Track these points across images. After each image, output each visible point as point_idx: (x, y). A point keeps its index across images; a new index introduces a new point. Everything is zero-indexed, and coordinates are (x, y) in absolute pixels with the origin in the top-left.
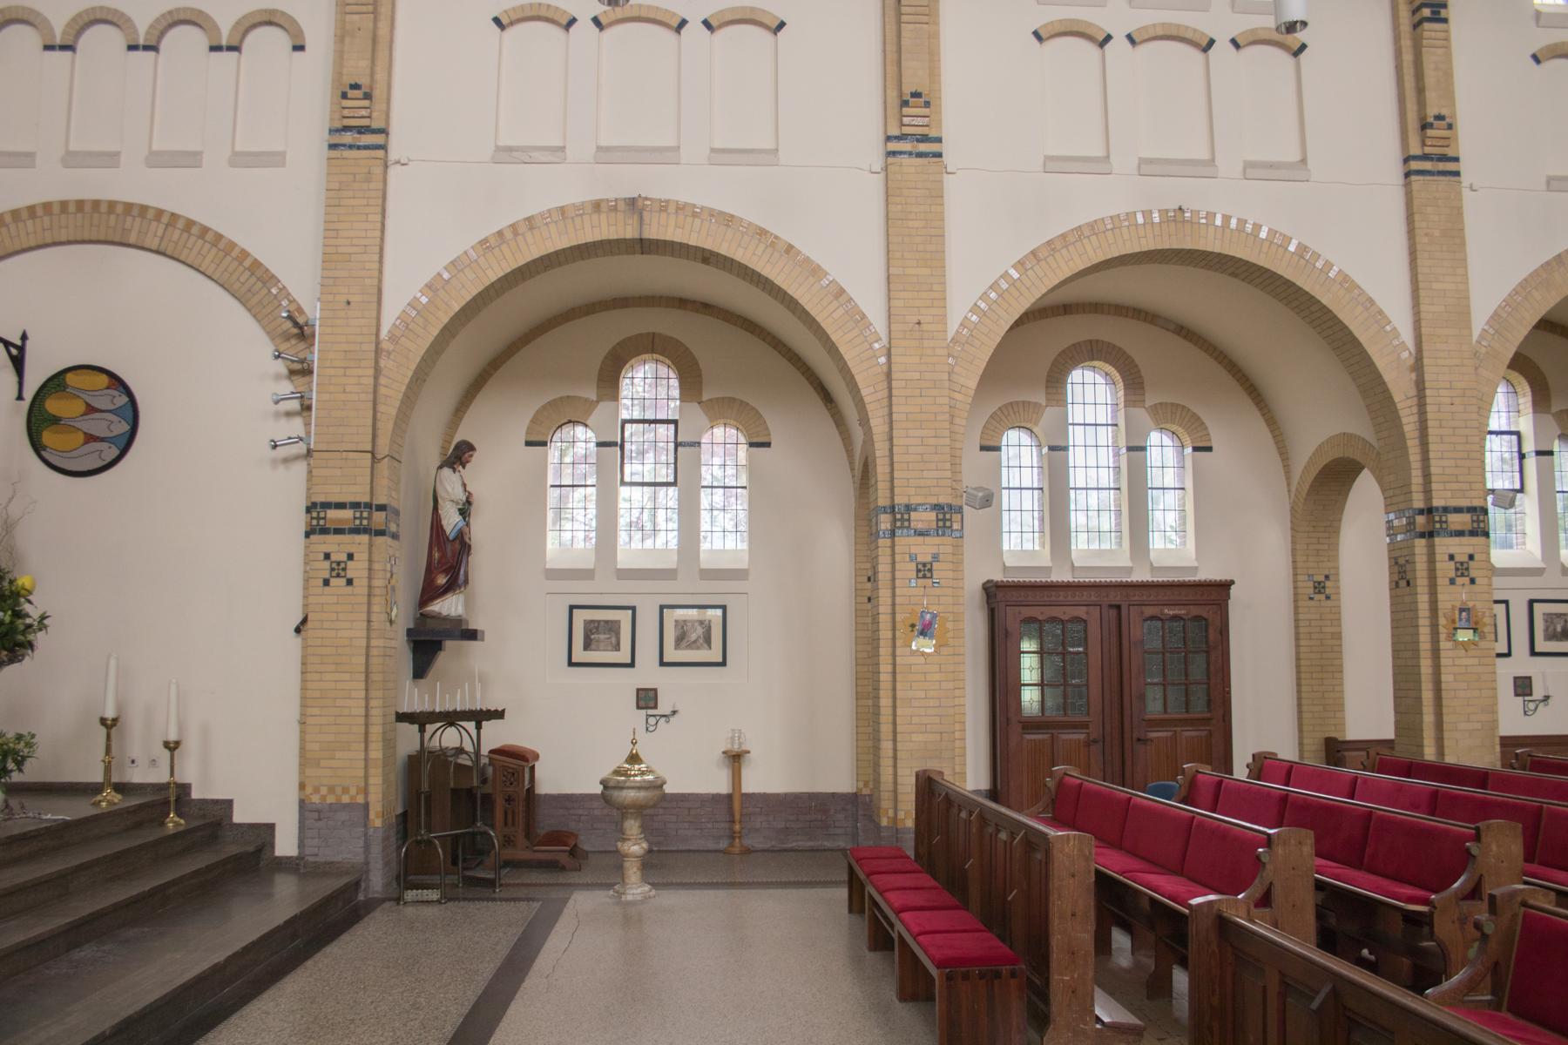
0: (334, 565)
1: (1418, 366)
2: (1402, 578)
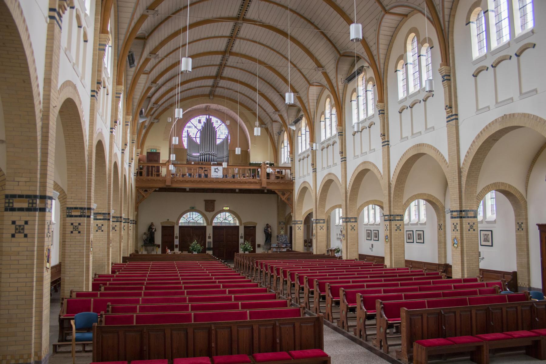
0: (74, 227)
2: (455, 225)
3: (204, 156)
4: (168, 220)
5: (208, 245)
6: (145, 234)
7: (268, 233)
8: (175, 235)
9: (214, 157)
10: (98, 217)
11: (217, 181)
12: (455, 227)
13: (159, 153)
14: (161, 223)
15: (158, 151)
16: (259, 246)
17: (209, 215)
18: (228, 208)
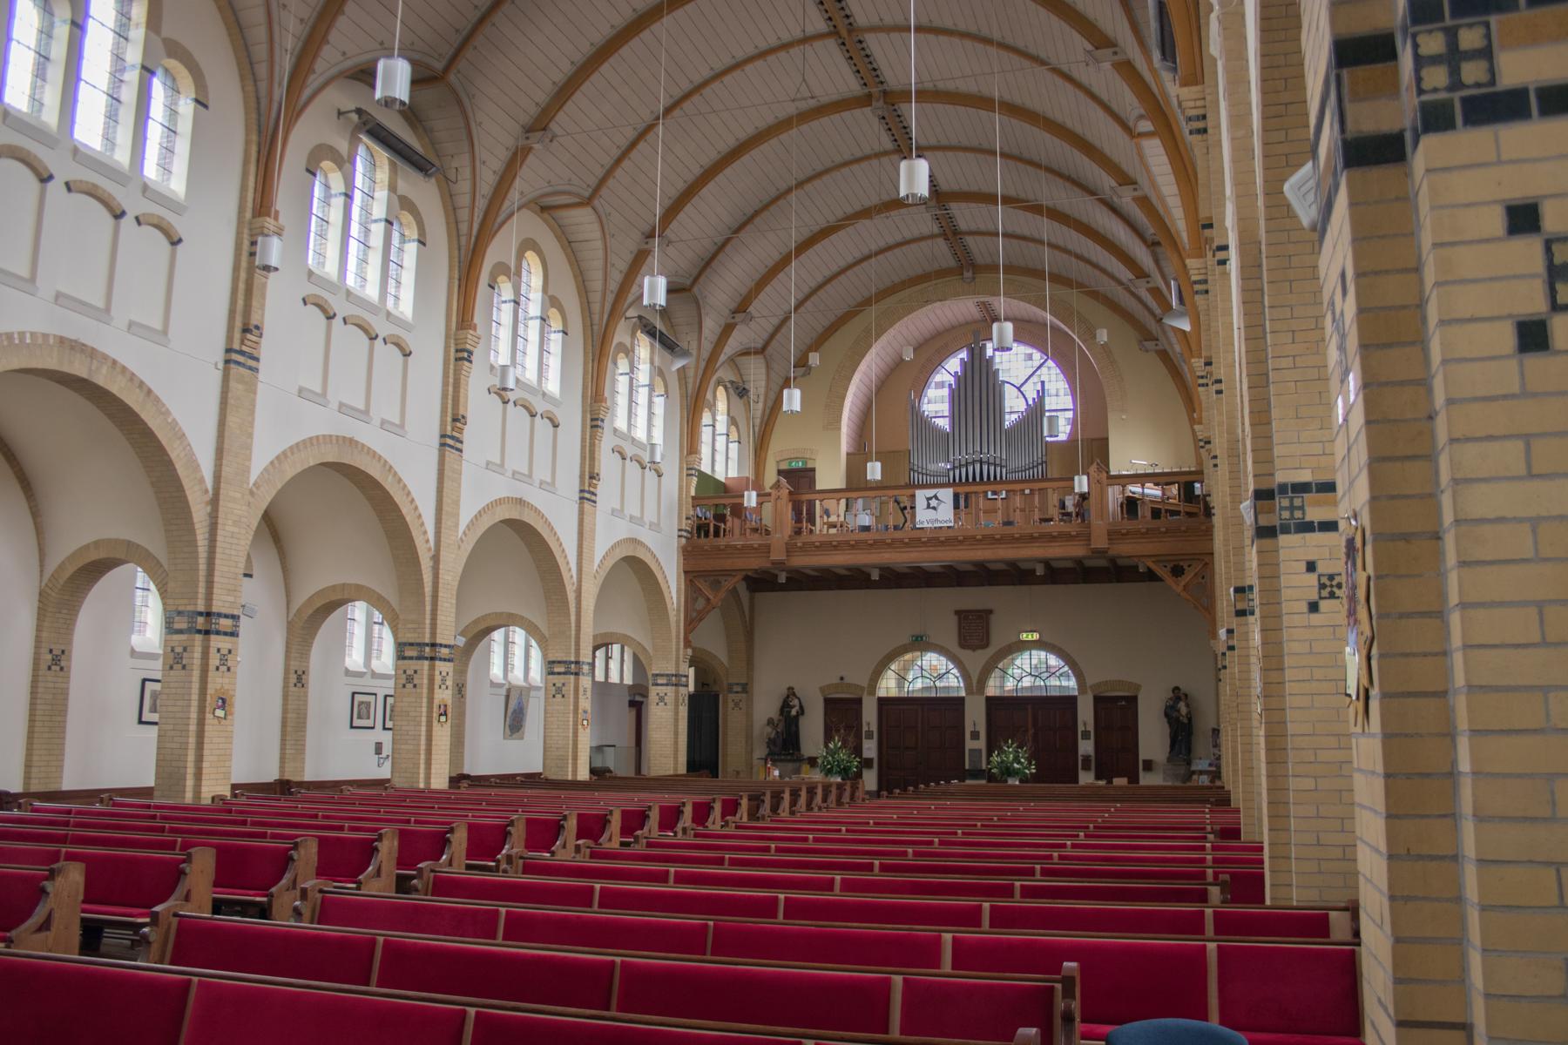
1: (215, 501)
3: (964, 470)
4: (842, 679)
5: (970, 760)
6: (770, 722)
7: (1177, 719)
8: (1081, 728)
9: (998, 469)
10: (556, 670)
11: (938, 539)
12: (224, 660)
13: (813, 470)
14: (822, 689)
15: (810, 465)
16: (1149, 766)
17: (977, 659)
18: (1036, 636)
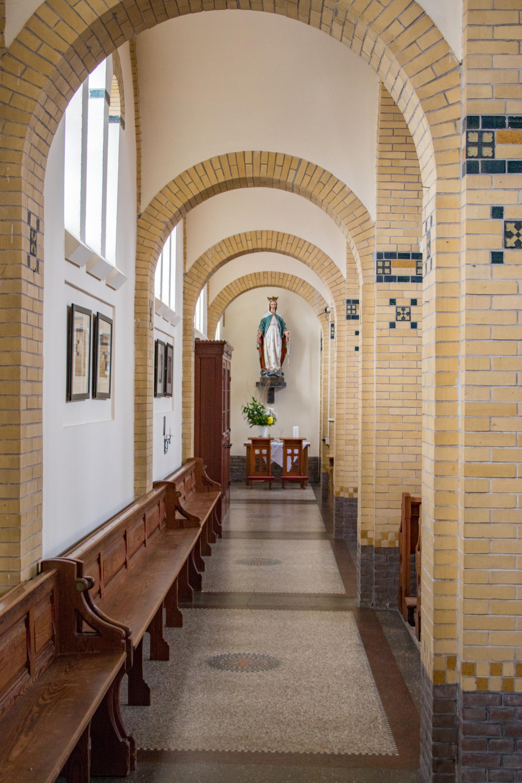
10: (396, 272)
